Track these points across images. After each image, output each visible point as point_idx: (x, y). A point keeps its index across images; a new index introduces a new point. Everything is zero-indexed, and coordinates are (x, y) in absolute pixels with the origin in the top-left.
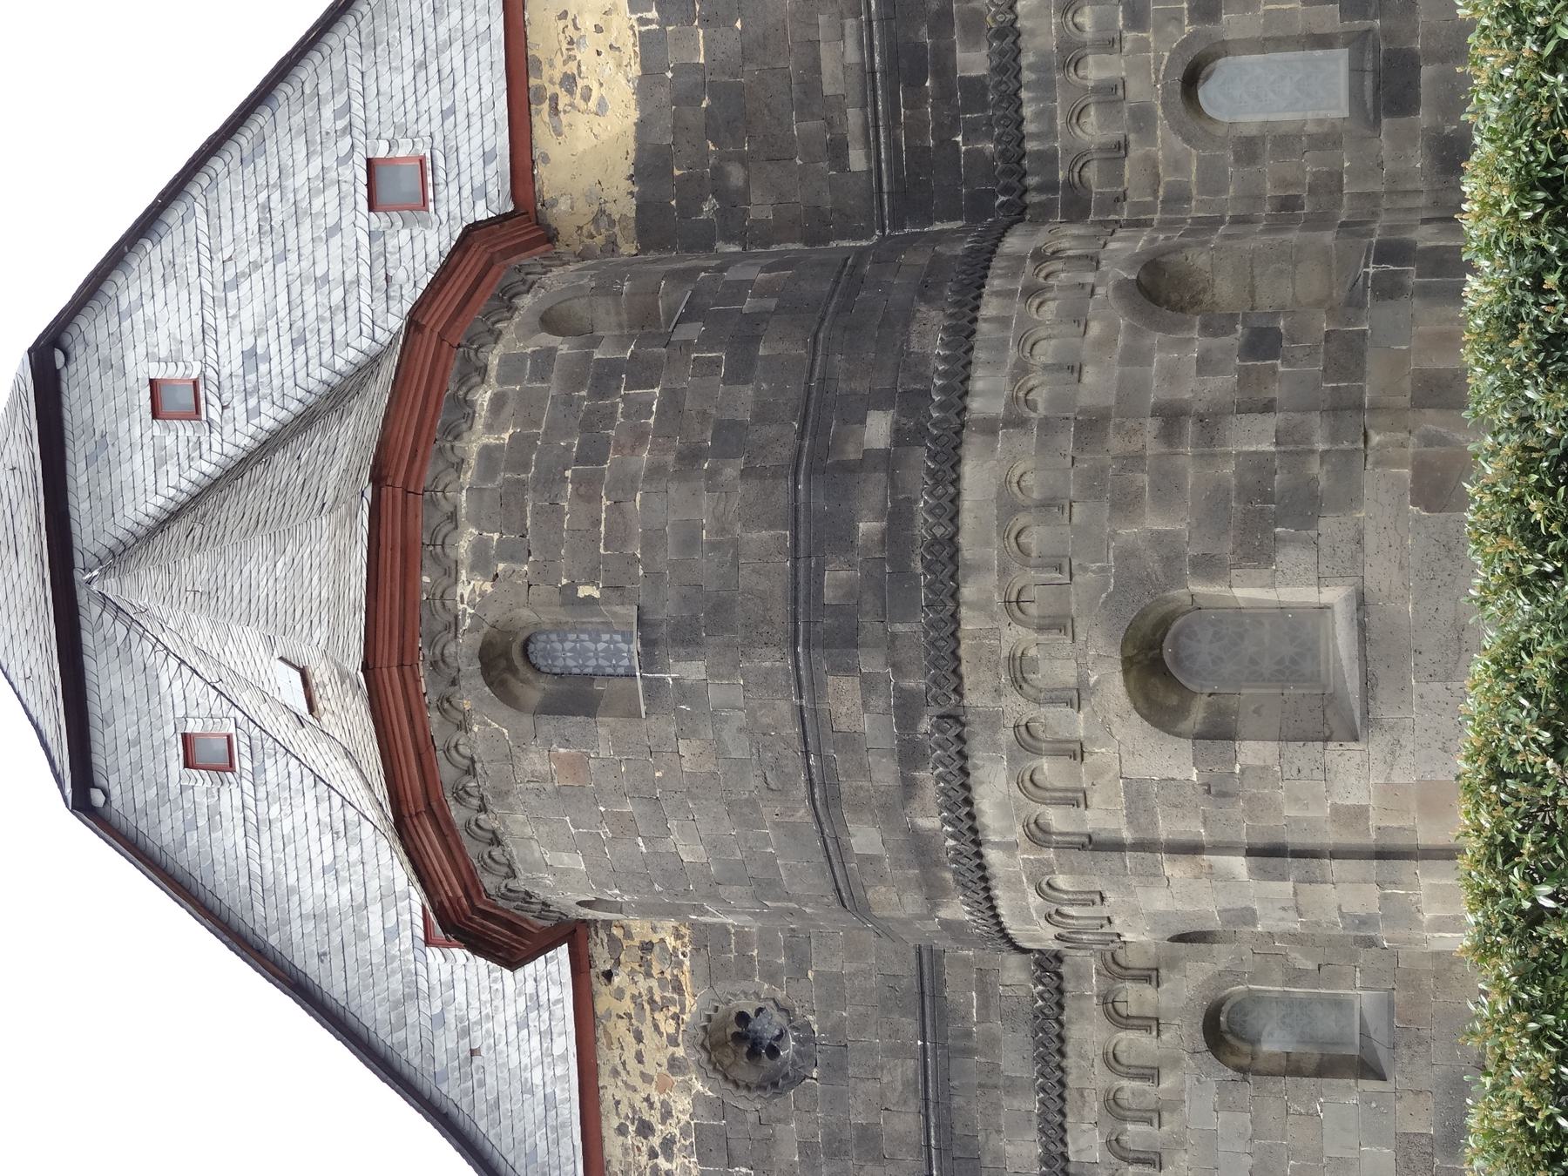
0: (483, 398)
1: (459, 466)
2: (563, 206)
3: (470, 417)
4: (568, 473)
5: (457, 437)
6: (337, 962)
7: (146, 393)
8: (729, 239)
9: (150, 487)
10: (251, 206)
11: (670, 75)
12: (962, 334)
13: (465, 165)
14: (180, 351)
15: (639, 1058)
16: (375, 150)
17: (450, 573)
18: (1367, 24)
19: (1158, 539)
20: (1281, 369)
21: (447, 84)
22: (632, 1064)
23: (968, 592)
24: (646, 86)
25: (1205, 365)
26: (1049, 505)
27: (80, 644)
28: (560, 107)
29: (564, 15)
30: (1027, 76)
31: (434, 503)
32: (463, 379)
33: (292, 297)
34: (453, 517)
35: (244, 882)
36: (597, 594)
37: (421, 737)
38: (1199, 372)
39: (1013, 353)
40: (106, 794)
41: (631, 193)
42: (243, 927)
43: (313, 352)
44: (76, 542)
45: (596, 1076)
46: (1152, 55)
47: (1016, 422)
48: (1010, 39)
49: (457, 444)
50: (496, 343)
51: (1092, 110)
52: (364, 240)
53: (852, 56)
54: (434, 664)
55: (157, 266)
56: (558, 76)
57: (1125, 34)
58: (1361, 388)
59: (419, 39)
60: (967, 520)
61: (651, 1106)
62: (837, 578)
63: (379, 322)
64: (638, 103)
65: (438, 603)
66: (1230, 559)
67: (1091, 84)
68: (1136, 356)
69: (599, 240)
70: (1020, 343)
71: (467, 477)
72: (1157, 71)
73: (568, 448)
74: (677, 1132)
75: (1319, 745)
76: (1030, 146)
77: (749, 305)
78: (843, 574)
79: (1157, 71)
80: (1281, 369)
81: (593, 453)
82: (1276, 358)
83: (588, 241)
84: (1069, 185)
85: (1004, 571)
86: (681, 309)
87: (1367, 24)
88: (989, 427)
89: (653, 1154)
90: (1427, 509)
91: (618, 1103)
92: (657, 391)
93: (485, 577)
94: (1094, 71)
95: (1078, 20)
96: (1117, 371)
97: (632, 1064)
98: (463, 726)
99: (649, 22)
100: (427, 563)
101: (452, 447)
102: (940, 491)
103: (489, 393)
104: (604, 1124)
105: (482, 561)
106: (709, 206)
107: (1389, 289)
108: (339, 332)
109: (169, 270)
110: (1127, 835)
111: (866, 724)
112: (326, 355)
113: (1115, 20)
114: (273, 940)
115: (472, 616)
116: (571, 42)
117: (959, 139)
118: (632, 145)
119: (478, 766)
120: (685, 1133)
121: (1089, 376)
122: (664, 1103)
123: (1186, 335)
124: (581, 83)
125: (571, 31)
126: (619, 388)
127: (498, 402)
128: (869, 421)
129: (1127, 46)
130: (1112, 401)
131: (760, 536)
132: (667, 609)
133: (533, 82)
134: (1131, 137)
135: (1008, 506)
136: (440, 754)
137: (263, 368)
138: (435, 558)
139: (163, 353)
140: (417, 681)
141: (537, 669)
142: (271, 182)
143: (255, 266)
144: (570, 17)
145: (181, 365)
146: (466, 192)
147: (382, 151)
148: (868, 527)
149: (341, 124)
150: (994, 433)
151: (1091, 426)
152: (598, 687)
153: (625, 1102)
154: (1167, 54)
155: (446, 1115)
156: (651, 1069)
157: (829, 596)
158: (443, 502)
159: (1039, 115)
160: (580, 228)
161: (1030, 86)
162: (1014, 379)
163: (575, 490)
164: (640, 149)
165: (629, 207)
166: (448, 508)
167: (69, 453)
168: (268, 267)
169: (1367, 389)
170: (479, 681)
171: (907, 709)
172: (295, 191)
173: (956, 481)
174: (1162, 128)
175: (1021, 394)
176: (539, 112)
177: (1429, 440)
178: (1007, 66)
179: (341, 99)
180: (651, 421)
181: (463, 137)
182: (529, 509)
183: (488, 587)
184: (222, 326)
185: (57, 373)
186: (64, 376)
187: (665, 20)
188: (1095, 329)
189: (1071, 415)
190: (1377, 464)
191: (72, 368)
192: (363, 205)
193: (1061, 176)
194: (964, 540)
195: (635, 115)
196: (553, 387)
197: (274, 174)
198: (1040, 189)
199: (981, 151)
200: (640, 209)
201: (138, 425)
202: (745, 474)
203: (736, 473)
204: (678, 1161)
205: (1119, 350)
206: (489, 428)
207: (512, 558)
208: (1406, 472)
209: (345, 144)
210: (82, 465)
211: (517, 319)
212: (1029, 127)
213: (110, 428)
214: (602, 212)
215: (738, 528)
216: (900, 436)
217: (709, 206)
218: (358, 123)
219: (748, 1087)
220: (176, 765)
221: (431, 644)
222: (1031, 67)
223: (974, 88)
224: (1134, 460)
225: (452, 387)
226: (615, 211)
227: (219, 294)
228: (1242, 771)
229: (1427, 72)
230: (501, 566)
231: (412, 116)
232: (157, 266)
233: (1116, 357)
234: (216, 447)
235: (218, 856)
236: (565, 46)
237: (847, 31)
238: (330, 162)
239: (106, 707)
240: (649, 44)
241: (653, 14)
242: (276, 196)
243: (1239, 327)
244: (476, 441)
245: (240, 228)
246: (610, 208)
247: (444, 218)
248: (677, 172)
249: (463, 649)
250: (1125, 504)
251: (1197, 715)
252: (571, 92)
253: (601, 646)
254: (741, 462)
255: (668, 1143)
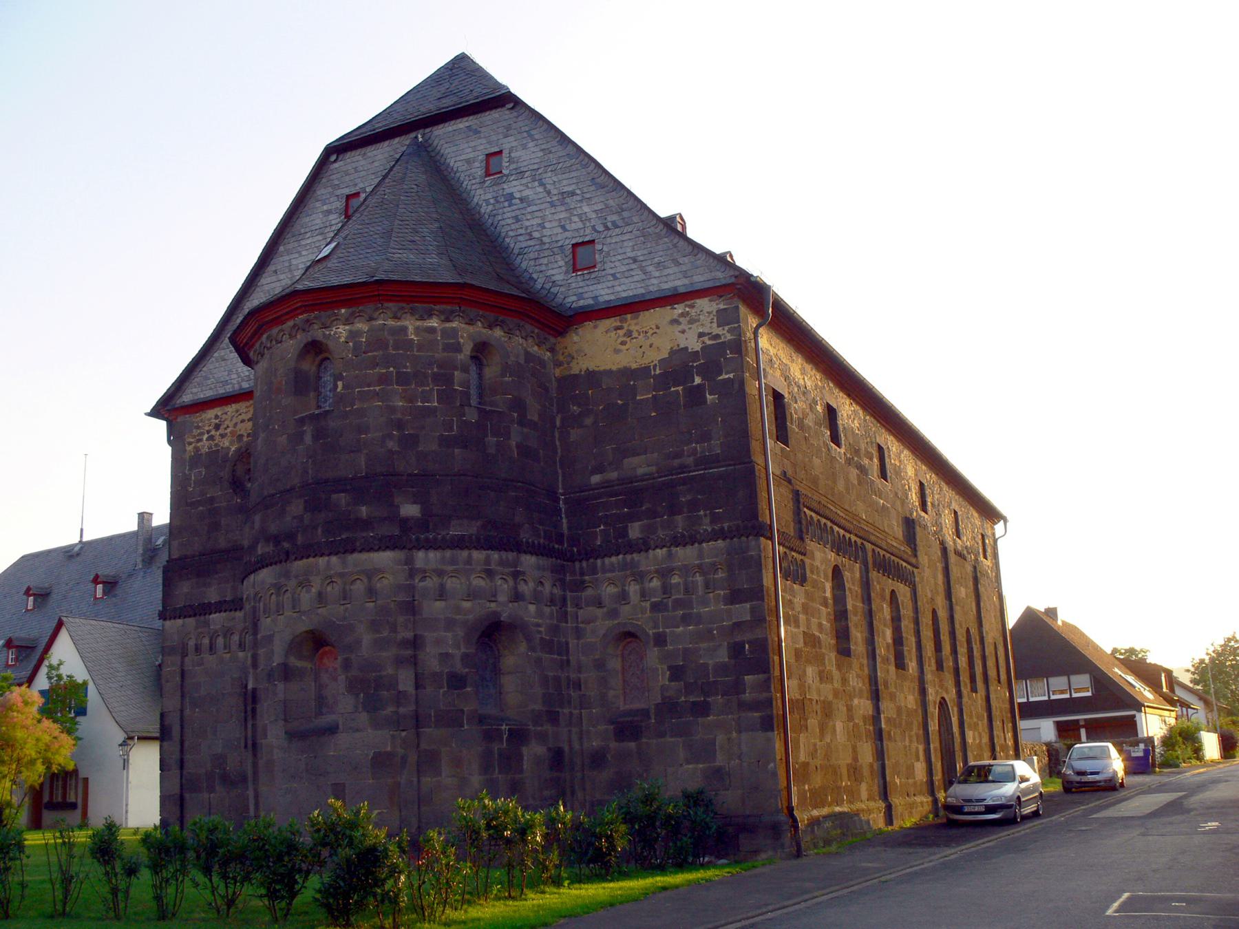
0: (434, 323)
1: (396, 317)
2: (576, 338)
3: (422, 318)
4: (391, 369)
5: (412, 314)
6: (274, 278)
7: (497, 149)
8: (563, 420)
9: (458, 159)
10: (573, 187)
11: (632, 383)
12: (459, 543)
13: (591, 288)
14: (514, 162)
15: (243, 421)
16: (598, 243)
17: (347, 322)
18: (653, 717)
19: (358, 642)
20: (441, 691)
21: (627, 274)
22: (241, 418)
23: (334, 559)
24: (627, 373)
25: (445, 657)
26: (371, 592)
27: (384, 141)
28: (618, 331)
29: (658, 328)
30: (629, 557)
31: (377, 309)
32: (442, 312)
33: (536, 213)
34: (371, 319)
35: (303, 231)
36: (339, 390)
37: (283, 318)
38: (441, 654)
39: (450, 568)
40: (335, 161)
41: (581, 371)
42: (285, 234)
43: (513, 227)
44: (435, 128)
45: (235, 402)
46: (640, 616)
47: (412, 573)
48: (643, 548)
49: (409, 315)
50: (466, 323)
51: (616, 590)
52: (560, 244)
53: (640, 471)
54: (308, 321)
55: (549, 145)
56: (632, 328)
57: (649, 602)
58: (431, 727)
59: (646, 257)
60: (364, 556)
61: (226, 429)
62: (342, 499)
63: (525, 256)
64: (619, 369)
65: (334, 318)
66: (349, 675)
67: (627, 588)
68: (450, 624)
69: (561, 358)
70: (456, 571)
71: (391, 323)
72: (632, 619)
73: (406, 367)
74: (216, 442)
75: (283, 717)
76: (599, 562)
77: (491, 440)
78: (343, 501)
79: (632, 619)
80: (441, 691)
81: (403, 379)
82: (448, 688)
83: (561, 352)
84: (583, 582)
85: (342, 575)
86: (488, 408)
87: (653, 717)
88: (409, 561)
89: (208, 432)
90: (372, 758)
91: (226, 413)
92: (436, 404)
93: (346, 338)
94: (633, 589)
95: (655, 580)
96: (442, 616)
97: (241, 418)
98: (291, 337)
99: (655, 370)
100: (350, 310)
101: (406, 313)
102: (376, 542)
103: (436, 325)
104: (219, 409)
105: (353, 335)
106: (575, 409)
107: (490, 736)
108: (521, 238)
109: (547, 152)
110: (259, 636)
111: (288, 519)
112: (511, 234)
113: (655, 597)
114: (282, 248)
115: (330, 334)
116: (646, 332)
117: (602, 527)
118: (602, 369)
119: (279, 345)
120: (216, 445)
121: (439, 605)
122: (226, 434)
123: (462, 647)
124: (628, 340)
125: (651, 332)
126: (438, 386)
127: (432, 330)
128: (415, 506)
129: (643, 604)
130: (424, 616)
131: (362, 460)
132: (332, 424)
133: (629, 316)
134: (605, 609)
135: (371, 574)
136: (280, 327)
137: (506, 204)
138: (352, 314)
139: (513, 155)
140: (301, 314)
141: (320, 365)
142: (584, 195)
143: (549, 193)
144: (657, 331)
145: (508, 164)
146: (580, 290)
147: (598, 247)
148: (364, 511)
149: (609, 225)
150: (406, 564)
151: (411, 608)
152: (312, 394)
153: (227, 417)
154: (640, 623)
155: (219, 337)
156: (240, 426)
157: (334, 496)
158: (378, 313)
159: (612, 564)
160: (566, 348)
161: (624, 559)
162: (434, 571)
163: (383, 374)
164: (600, 372)
165: (575, 371)
166: (375, 316)
167: (471, 118)
168: (548, 199)
169: (431, 729)
170: (305, 341)
171: (291, 537)
172: (580, 207)
173: (379, 549)
174: (609, 623)
175: (428, 574)
176: (615, 321)
177: (404, 759)
178: (632, 547)
179: (620, 223)
180: (420, 404)
181: (604, 285)
182: (375, 353)
183: (343, 339)
184: (524, 181)
185: (503, 106)
186: (504, 109)
187: (655, 377)
188: (467, 605)
189: (416, 598)
190: (393, 736)
191: (507, 112)
192: (574, 241)
193: (587, 578)
194: (356, 556)
195: (614, 368)
196: (440, 355)
197: (588, 196)
198: (581, 568)
199: (596, 538)
200: (575, 375)
201: (482, 147)
202: (391, 452)
203: (390, 447)
204: (207, 444)
205: (454, 617)
206: (417, 329)
207: (355, 348)
208: (389, 749)
209: (601, 228)
210: (467, 124)
211: (484, 331)
212: (607, 560)
213: (482, 135)
214: (573, 358)
215: (365, 452)
216: (404, 521)
217: (575, 409)
218: (610, 232)
219: (234, 471)
220: (347, 191)
221: (316, 318)
222: (633, 559)
223: (623, 533)
224: (394, 629)
225: (437, 307)
226: (573, 364)
227: (537, 177)
228: (275, 685)
229: (632, 745)
230: (351, 344)
231: (613, 259)
232: (549, 145)
233: (450, 616)
234: (474, 187)
235: (312, 218)
236: (644, 330)
237: (650, 468)
238: (593, 223)
239: (369, 154)
240: (644, 371)
241: (658, 372)
242: (579, 198)
243: (467, 670)
244: (410, 324)
245: (565, 182)
246: (575, 361)
247: (569, 281)
248: (590, 392)
249: (317, 333)
250: (374, 626)
251: (295, 662)
252: (624, 335)
253: (328, 393)
254: (396, 448)
255: (211, 438)
